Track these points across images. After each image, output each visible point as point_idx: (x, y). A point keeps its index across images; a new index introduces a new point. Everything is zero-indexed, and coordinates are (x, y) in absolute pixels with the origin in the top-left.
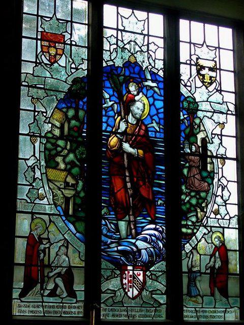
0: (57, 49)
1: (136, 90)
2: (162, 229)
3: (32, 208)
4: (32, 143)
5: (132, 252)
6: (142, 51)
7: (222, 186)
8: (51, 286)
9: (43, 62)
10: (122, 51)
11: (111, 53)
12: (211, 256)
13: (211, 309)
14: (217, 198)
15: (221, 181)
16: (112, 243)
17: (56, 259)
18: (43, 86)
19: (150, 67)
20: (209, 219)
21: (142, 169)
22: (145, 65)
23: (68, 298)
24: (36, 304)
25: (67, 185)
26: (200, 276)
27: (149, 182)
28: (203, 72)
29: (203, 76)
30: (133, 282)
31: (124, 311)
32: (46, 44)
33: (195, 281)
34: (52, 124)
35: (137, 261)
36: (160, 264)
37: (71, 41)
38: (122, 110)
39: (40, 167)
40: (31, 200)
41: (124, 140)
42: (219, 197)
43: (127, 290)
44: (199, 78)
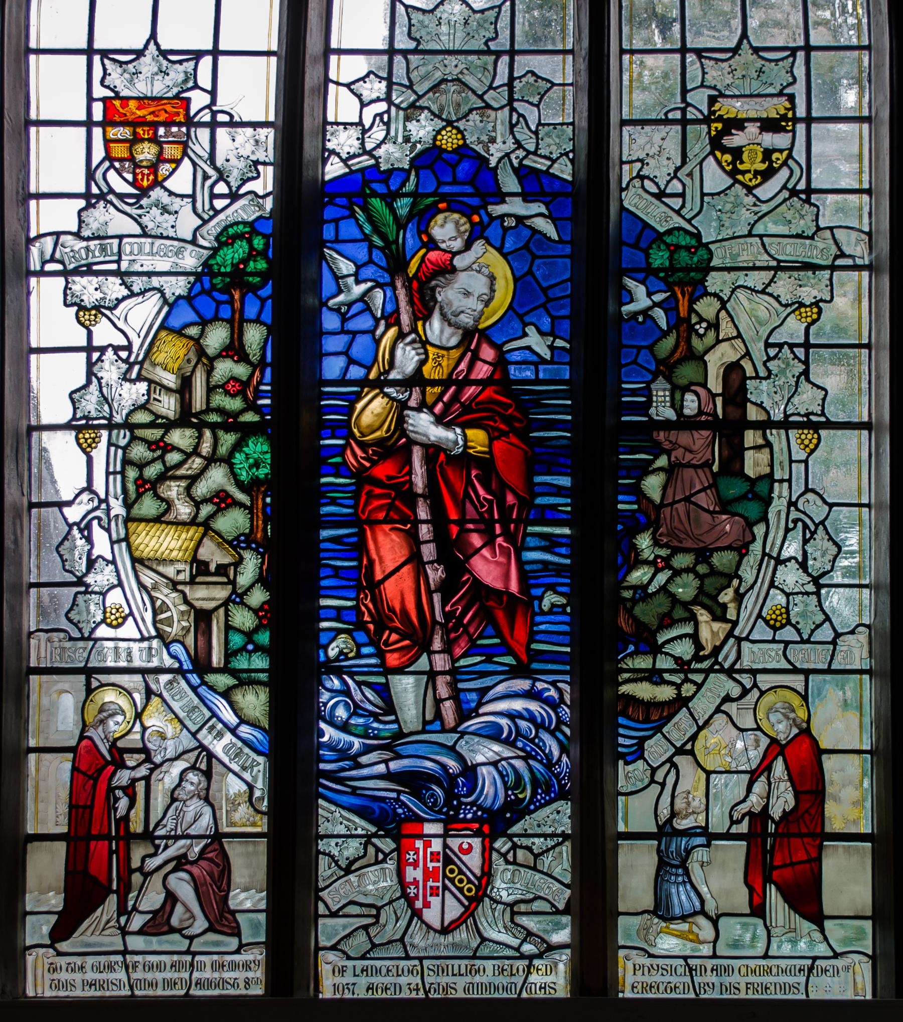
0: (160, 144)
1: (460, 234)
2: (560, 691)
3: (85, 655)
4: (84, 450)
5: (448, 781)
6: (488, 106)
7: (805, 526)
8: (153, 899)
9: (111, 191)
10: (407, 119)
11: (364, 131)
12: (754, 775)
13: (752, 963)
14: (781, 568)
15: (800, 506)
16: (368, 750)
17: (171, 812)
18: (114, 267)
19: (521, 153)
20: (745, 645)
21: (482, 492)
22: (495, 154)
23: (211, 937)
24: (103, 959)
25: (200, 568)
26: (708, 845)
27: (506, 534)
28: (736, 139)
29: (737, 153)
30: (445, 876)
31: (411, 972)
32: (123, 132)
33: (683, 865)
34: (150, 382)
35: (460, 803)
36: (547, 810)
37: (214, 114)
38: (438, 758)
39: (109, 521)
40: (80, 630)
41: (413, 403)
42: (792, 565)
43: (419, 904)
44: (719, 163)
